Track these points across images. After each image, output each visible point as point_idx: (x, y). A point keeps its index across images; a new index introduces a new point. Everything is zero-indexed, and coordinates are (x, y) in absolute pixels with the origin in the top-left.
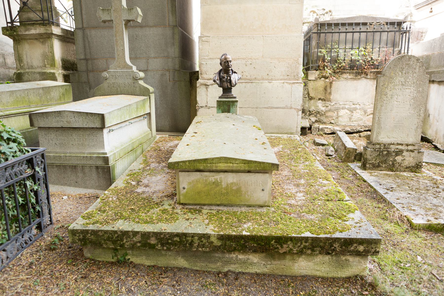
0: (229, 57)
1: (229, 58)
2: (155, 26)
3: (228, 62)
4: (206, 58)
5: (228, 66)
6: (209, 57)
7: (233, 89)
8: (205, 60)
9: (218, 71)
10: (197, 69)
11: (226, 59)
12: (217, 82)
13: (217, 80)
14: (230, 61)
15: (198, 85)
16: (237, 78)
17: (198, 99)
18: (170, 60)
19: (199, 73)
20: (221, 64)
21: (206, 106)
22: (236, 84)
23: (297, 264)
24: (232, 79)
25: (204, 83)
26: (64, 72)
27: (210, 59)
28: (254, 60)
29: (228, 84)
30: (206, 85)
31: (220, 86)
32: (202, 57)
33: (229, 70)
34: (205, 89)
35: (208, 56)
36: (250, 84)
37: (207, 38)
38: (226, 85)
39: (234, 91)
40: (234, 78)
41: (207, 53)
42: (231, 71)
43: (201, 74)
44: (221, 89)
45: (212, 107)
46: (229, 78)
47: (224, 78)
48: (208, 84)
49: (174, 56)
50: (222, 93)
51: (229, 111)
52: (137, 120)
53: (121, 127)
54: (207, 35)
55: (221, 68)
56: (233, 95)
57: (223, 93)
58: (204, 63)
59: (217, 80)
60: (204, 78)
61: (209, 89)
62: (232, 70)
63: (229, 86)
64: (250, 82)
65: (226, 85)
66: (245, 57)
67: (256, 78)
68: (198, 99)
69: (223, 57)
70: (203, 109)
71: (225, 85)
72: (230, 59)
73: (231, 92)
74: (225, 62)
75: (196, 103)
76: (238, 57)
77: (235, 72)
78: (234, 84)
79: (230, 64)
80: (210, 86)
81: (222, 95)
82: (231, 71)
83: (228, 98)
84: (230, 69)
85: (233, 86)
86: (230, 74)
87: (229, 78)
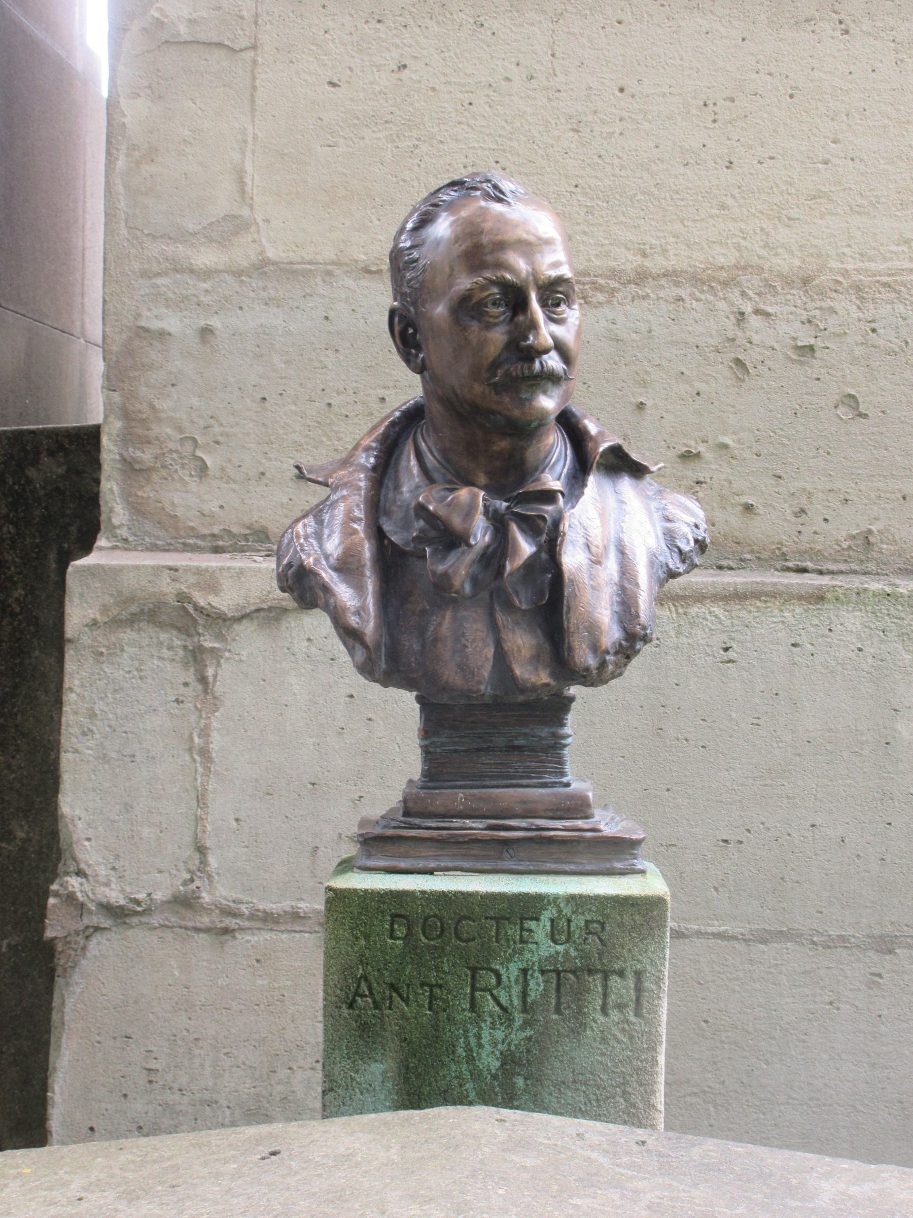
0: (542, 233)
1: (528, 247)
3: (515, 298)
5: (520, 364)
6: (242, 253)
7: (593, 724)
9: (357, 430)
10: (94, 408)
11: (479, 250)
12: (344, 593)
13: (346, 567)
14: (554, 293)
15: (78, 613)
16: (644, 541)
17: (70, 804)
19: (110, 450)
20: (407, 333)
21: (185, 902)
22: (633, 640)
23: (349, 604)
24: (572, 559)
25: (167, 588)
27: (261, 267)
28: (846, 306)
29: (522, 642)
30: (192, 626)
31: (390, 658)
32: (154, 249)
33: (525, 430)
36: (794, 613)
38: (476, 635)
39: (601, 745)
40: (610, 535)
41: (223, 202)
42: (556, 450)
44: (405, 704)
45: (268, 919)
46: (526, 548)
47: (451, 539)
48: (225, 601)
50: (409, 763)
55: (406, 388)
56: (578, 807)
57: (437, 769)
58: (172, 323)
59: (346, 567)
61: (224, 676)
62: (568, 423)
63: (533, 674)
64: (786, 597)
65: (483, 655)
66: (725, 257)
67: (866, 540)
68: (75, 804)
69: (443, 228)
70: (138, 936)
71: (482, 648)
72: (555, 262)
73: (551, 752)
74: (468, 308)
75: (47, 851)
76: (629, 261)
77: (621, 464)
78: (612, 634)
79: (546, 332)
81: (411, 809)
82: (556, 450)
83: (496, 852)
84: (548, 403)
85: (587, 678)
86: (553, 481)
87: (526, 548)
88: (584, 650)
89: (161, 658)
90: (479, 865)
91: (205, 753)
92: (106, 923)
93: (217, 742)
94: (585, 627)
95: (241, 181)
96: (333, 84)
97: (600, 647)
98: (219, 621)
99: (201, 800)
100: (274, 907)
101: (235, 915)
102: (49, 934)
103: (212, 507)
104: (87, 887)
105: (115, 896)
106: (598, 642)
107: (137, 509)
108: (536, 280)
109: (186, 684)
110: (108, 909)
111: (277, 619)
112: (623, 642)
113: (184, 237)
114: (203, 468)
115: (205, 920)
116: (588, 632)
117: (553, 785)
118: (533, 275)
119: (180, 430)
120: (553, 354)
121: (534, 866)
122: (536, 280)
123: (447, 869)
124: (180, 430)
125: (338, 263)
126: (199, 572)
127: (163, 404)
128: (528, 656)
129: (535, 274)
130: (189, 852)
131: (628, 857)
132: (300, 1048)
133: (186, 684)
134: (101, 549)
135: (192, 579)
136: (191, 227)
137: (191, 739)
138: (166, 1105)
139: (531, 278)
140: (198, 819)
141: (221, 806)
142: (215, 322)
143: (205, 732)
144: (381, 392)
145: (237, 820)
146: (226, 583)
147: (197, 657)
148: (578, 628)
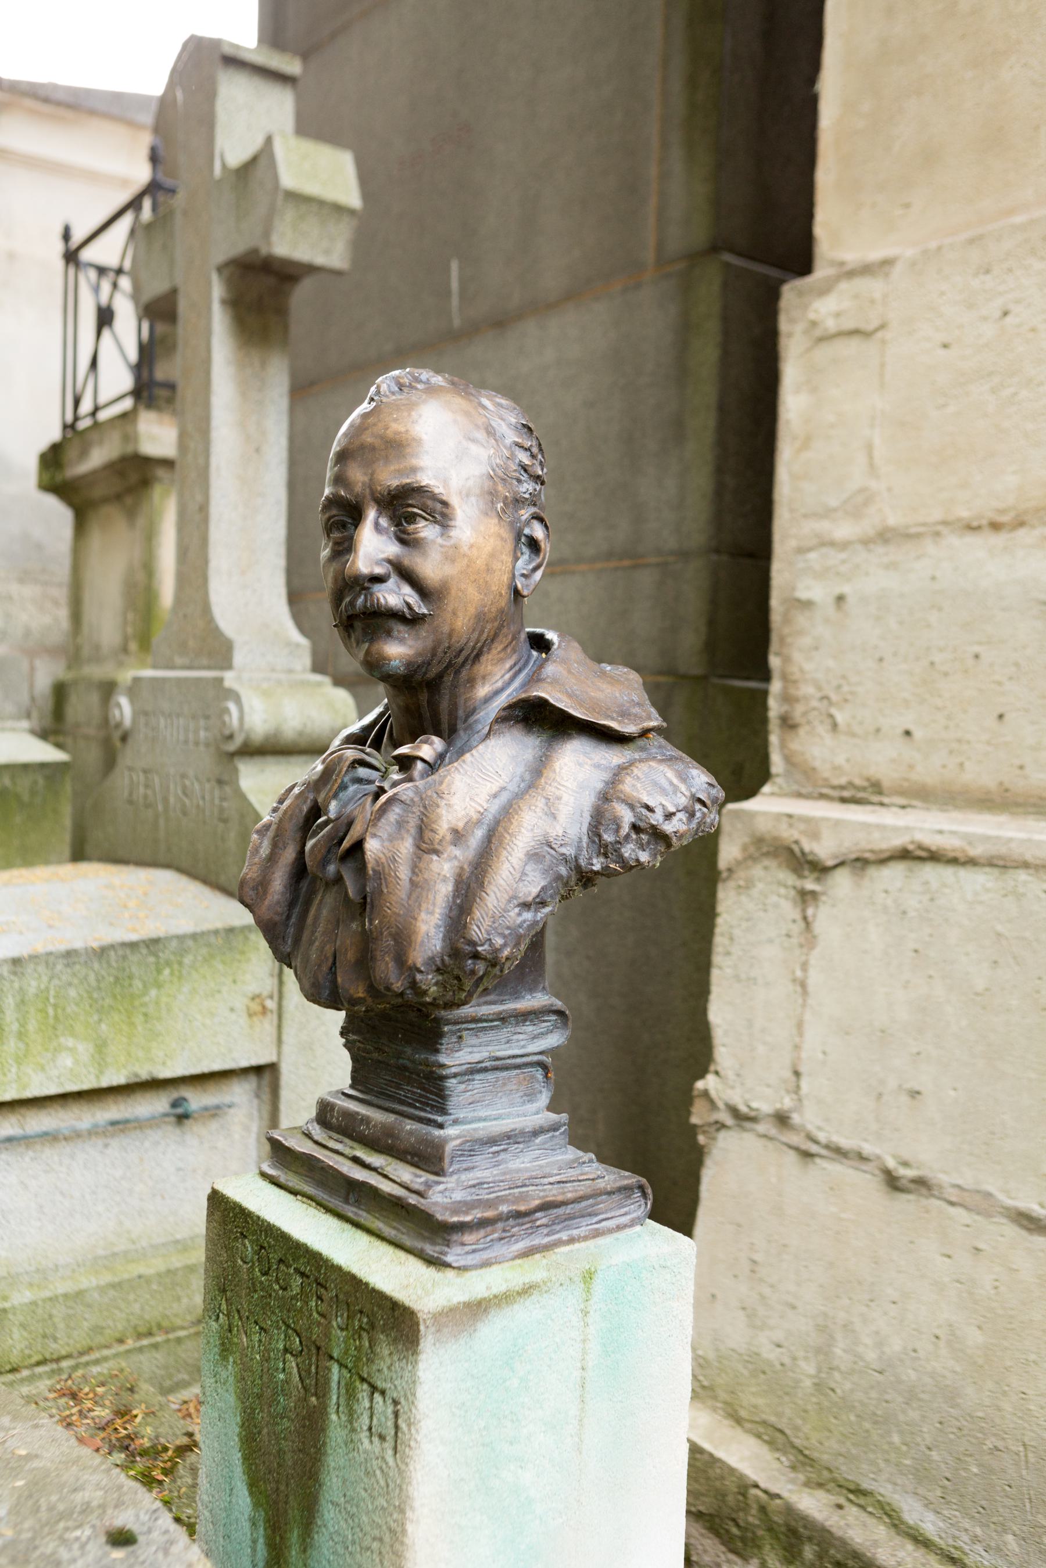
2: (571, 296)
4: (843, 530)
6: (866, 527)
8: (835, 557)
18: (646, 579)
26: (230, 679)
27: (885, 536)
34: (790, 910)
35: (858, 504)
37: (862, 284)
43: (788, 724)
45: (839, 1152)
48: (824, 850)
49: (672, 543)
51: (695, 1396)
52: (84, 1117)
53: (51, 1137)
54: (875, 255)
60: (809, 773)
61: (823, 916)
80: (842, 881)
88: (387, 963)
89: (779, 896)
90: (335, 1203)
91: (803, 985)
92: (729, 1121)
93: (814, 978)
94: (390, 934)
95: (871, 457)
96: (945, 346)
97: (407, 961)
98: (820, 869)
99: (800, 1025)
100: (845, 1143)
101: (816, 1142)
102: (694, 1120)
103: (840, 760)
104: (720, 1087)
105: (737, 1098)
106: (405, 954)
107: (788, 759)
108: (373, 493)
109: (794, 921)
110: (734, 1112)
111: (863, 869)
112: (446, 958)
113: (828, 513)
114: (835, 726)
115: (795, 1139)
116: (395, 940)
117: (429, 1122)
118: (371, 489)
119: (819, 688)
120: (393, 581)
121: (356, 1214)
122: (373, 493)
123: (310, 1198)
124: (819, 688)
125: (945, 523)
126: (807, 820)
127: (808, 666)
128: (353, 960)
129: (371, 485)
130: (788, 1074)
131: (440, 1241)
132: (860, 1283)
133: (794, 921)
134: (764, 794)
135: (802, 826)
136: (833, 503)
137: (793, 972)
138: (763, 1297)
139: (368, 490)
140: (797, 1047)
141: (814, 1037)
142: (846, 589)
143: (805, 966)
144: (977, 649)
145: (824, 1053)
146: (826, 834)
147: (805, 897)
148: (382, 934)
